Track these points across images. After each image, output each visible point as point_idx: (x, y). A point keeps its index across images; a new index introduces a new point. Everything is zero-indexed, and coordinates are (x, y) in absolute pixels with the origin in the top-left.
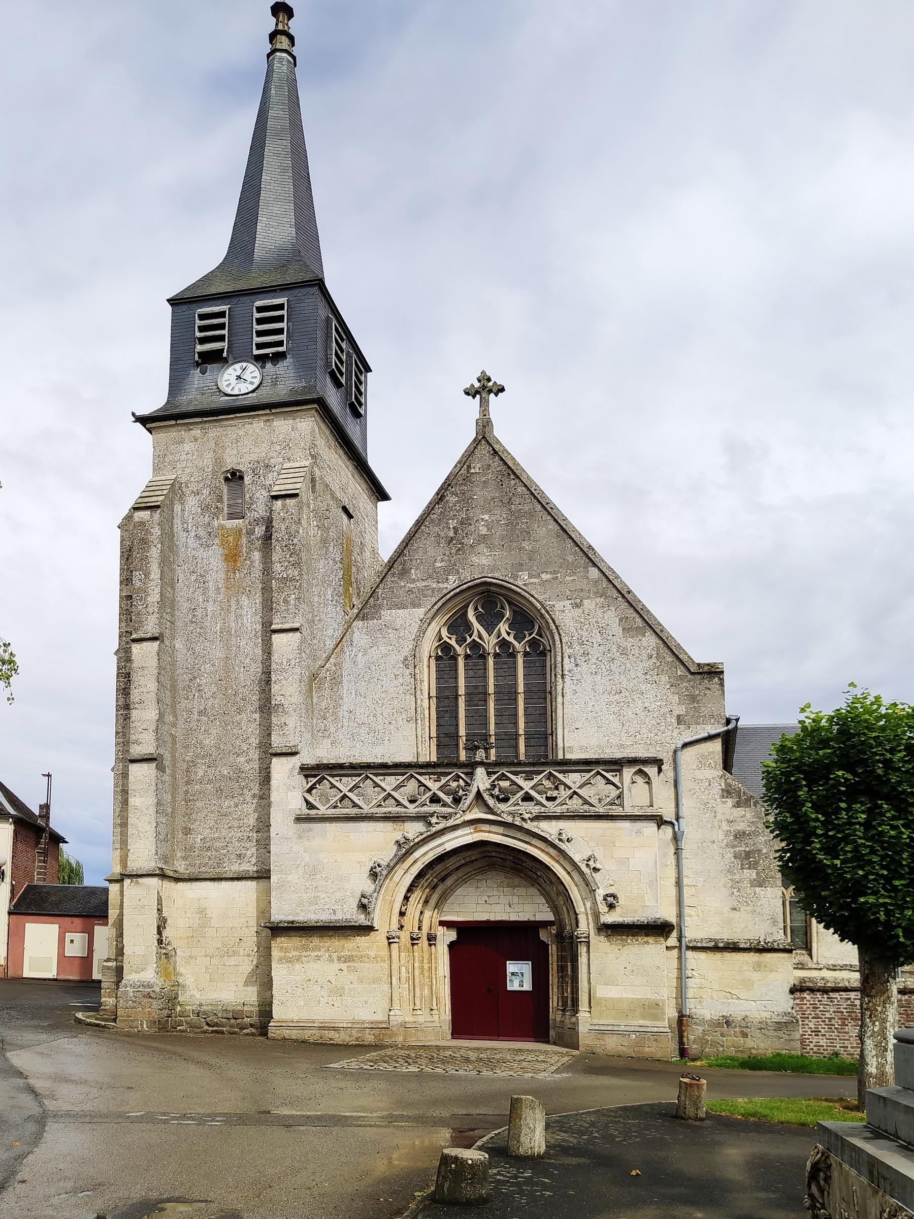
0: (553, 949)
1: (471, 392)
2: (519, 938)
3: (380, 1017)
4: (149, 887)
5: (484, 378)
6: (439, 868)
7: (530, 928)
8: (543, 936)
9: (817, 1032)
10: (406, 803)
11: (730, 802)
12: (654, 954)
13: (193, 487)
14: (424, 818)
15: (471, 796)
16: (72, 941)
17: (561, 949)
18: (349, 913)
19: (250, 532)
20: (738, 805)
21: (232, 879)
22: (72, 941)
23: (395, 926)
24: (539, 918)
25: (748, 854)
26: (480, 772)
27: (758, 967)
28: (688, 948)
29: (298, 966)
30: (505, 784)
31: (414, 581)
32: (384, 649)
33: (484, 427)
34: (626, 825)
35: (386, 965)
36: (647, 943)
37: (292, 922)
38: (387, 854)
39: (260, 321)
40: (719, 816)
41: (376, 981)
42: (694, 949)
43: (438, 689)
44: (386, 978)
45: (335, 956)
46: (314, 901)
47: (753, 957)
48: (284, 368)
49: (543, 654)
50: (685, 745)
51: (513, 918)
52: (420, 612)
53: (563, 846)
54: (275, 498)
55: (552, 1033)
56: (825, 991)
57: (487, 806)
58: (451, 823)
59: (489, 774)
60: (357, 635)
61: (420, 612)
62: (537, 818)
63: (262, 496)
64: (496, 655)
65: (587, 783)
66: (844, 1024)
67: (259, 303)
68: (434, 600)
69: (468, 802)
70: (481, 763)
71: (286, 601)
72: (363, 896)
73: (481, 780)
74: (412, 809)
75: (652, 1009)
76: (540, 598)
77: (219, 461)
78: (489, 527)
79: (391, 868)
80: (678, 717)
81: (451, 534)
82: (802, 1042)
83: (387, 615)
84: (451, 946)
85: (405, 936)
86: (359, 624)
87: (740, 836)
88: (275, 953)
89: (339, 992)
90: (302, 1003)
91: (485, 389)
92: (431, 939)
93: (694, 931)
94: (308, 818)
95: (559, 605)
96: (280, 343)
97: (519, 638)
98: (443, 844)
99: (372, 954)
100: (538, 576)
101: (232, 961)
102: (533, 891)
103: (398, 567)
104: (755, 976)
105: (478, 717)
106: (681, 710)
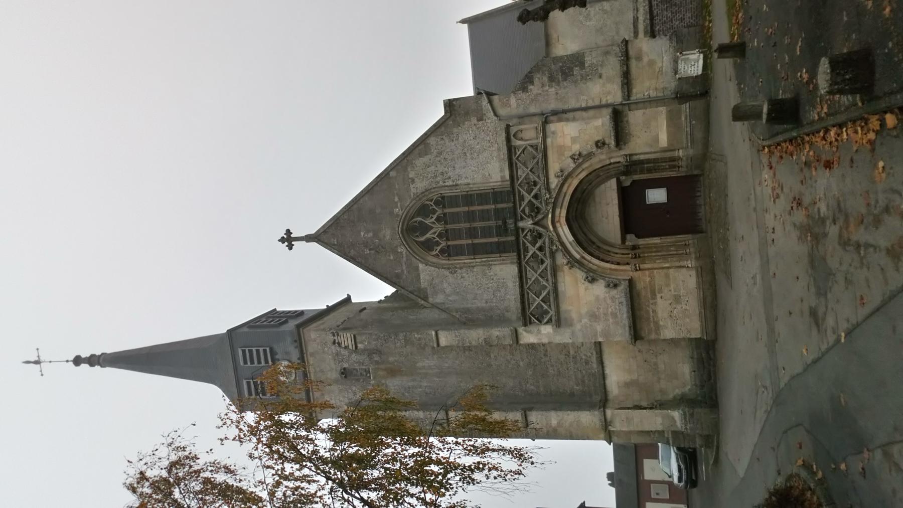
0: (636, 177)
1: (290, 247)
2: (630, 199)
3: (693, 273)
4: (613, 415)
5: (282, 240)
6: (585, 244)
7: (623, 192)
8: (627, 183)
9: (682, 20)
10: (544, 265)
11: (531, 87)
12: (635, 118)
13: (351, 395)
14: (553, 254)
15: (537, 228)
16: (657, 494)
17: (635, 172)
18: (619, 294)
19: (377, 362)
20: (532, 83)
21: (603, 367)
22: (657, 494)
23: (627, 267)
24: (615, 186)
25: (563, 73)
26: (521, 224)
27: (639, 58)
28: (629, 99)
29: (661, 323)
30: (527, 211)
31: (402, 271)
32: (445, 285)
33: (309, 238)
34: (549, 141)
35: (655, 271)
36: (627, 121)
37: (630, 327)
38: (580, 274)
39: (252, 362)
40: (540, 92)
41: (667, 276)
42: (629, 96)
43: (469, 254)
44: (665, 270)
45: (652, 301)
46: (614, 315)
47: (633, 63)
48: (278, 348)
49: (443, 198)
50: (495, 114)
51: (616, 201)
52: (421, 266)
53: (566, 173)
54: (356, 347)
55: (696, 172)
56: (652, 18)
57: (543, 218)
58: (555, 238)
59: (522, 219)
60: (438, 301)
61: (421, 266)
62: (548, 189)
63: (354, 357)
64: (446, 223)
65: (525, 164)
66: (675, 5)
67: (242, 363)
68: (413, 259)
69: (541, 229)
70: (516, 224)
71: (420, 339)
72: (609, 286)
73: (528, 224)
74: (548, 261)
75: (673, 120)
76: (409, 201)
77: (336, 381)
78: (368, 231)
79: (589, 271)
80: (478, 120)
81: (373, 252)
82: (689, 27)
83: (424, 284)
84: (638, 236)
85: (633, 261)
86: (431, 300)
87: (552, 79)
88: (653, 336)
89: (677, 299)
90: (688, 320)
91: (288, 239)
92: (634, 247)
93: (615, 96)
94: (558, 322)
95: (413, 190)
96: (265, 351)
97: (434, 212)
98: (570, 243)
99: (648, 279)
100: (396, 203)
101: (662, 367)
102: (597, 192)
103: (394, 280)
104: (645, 59)
105: (486, 232)
106: (474, 120)
